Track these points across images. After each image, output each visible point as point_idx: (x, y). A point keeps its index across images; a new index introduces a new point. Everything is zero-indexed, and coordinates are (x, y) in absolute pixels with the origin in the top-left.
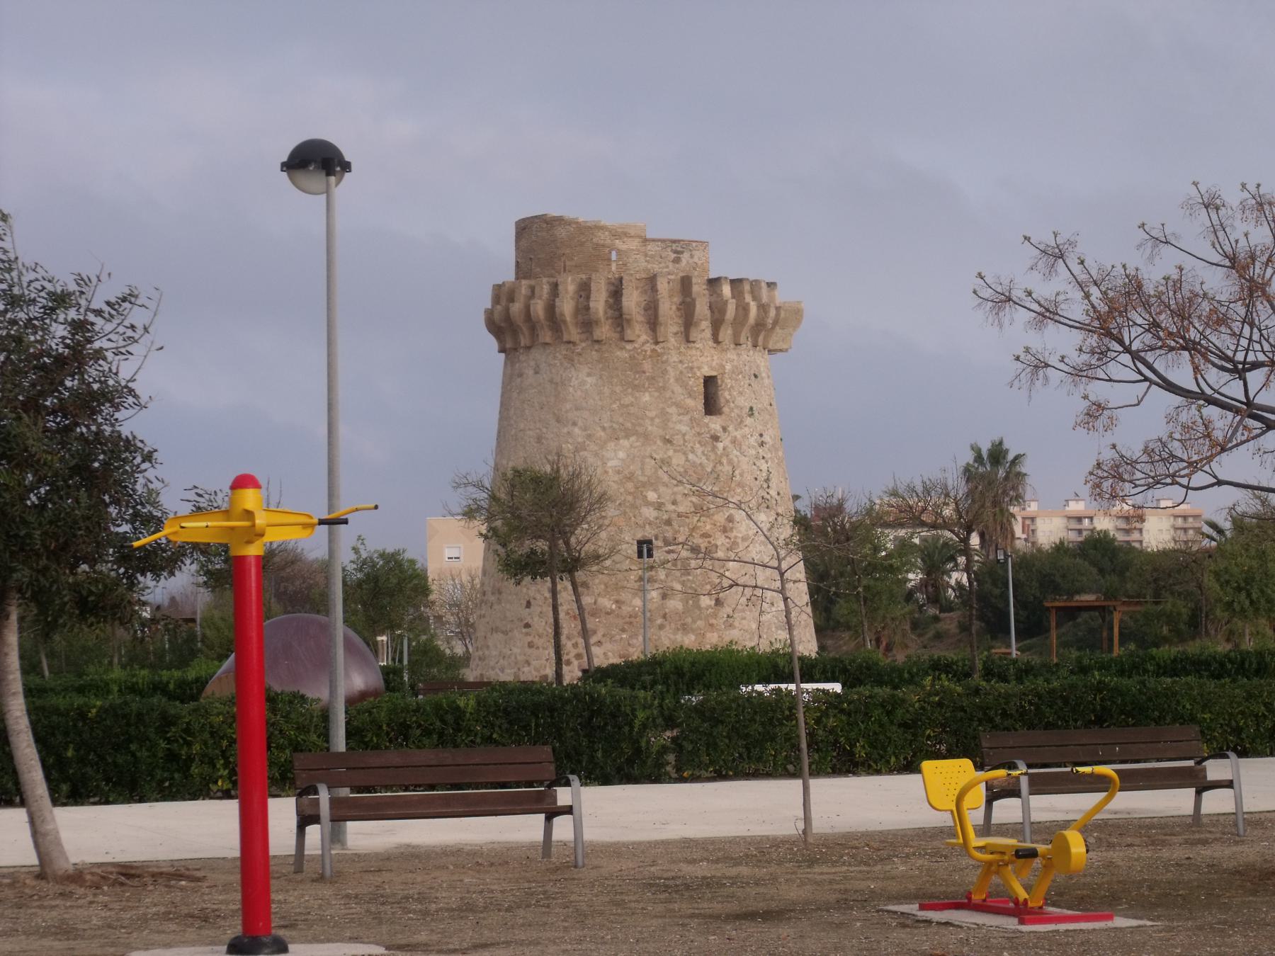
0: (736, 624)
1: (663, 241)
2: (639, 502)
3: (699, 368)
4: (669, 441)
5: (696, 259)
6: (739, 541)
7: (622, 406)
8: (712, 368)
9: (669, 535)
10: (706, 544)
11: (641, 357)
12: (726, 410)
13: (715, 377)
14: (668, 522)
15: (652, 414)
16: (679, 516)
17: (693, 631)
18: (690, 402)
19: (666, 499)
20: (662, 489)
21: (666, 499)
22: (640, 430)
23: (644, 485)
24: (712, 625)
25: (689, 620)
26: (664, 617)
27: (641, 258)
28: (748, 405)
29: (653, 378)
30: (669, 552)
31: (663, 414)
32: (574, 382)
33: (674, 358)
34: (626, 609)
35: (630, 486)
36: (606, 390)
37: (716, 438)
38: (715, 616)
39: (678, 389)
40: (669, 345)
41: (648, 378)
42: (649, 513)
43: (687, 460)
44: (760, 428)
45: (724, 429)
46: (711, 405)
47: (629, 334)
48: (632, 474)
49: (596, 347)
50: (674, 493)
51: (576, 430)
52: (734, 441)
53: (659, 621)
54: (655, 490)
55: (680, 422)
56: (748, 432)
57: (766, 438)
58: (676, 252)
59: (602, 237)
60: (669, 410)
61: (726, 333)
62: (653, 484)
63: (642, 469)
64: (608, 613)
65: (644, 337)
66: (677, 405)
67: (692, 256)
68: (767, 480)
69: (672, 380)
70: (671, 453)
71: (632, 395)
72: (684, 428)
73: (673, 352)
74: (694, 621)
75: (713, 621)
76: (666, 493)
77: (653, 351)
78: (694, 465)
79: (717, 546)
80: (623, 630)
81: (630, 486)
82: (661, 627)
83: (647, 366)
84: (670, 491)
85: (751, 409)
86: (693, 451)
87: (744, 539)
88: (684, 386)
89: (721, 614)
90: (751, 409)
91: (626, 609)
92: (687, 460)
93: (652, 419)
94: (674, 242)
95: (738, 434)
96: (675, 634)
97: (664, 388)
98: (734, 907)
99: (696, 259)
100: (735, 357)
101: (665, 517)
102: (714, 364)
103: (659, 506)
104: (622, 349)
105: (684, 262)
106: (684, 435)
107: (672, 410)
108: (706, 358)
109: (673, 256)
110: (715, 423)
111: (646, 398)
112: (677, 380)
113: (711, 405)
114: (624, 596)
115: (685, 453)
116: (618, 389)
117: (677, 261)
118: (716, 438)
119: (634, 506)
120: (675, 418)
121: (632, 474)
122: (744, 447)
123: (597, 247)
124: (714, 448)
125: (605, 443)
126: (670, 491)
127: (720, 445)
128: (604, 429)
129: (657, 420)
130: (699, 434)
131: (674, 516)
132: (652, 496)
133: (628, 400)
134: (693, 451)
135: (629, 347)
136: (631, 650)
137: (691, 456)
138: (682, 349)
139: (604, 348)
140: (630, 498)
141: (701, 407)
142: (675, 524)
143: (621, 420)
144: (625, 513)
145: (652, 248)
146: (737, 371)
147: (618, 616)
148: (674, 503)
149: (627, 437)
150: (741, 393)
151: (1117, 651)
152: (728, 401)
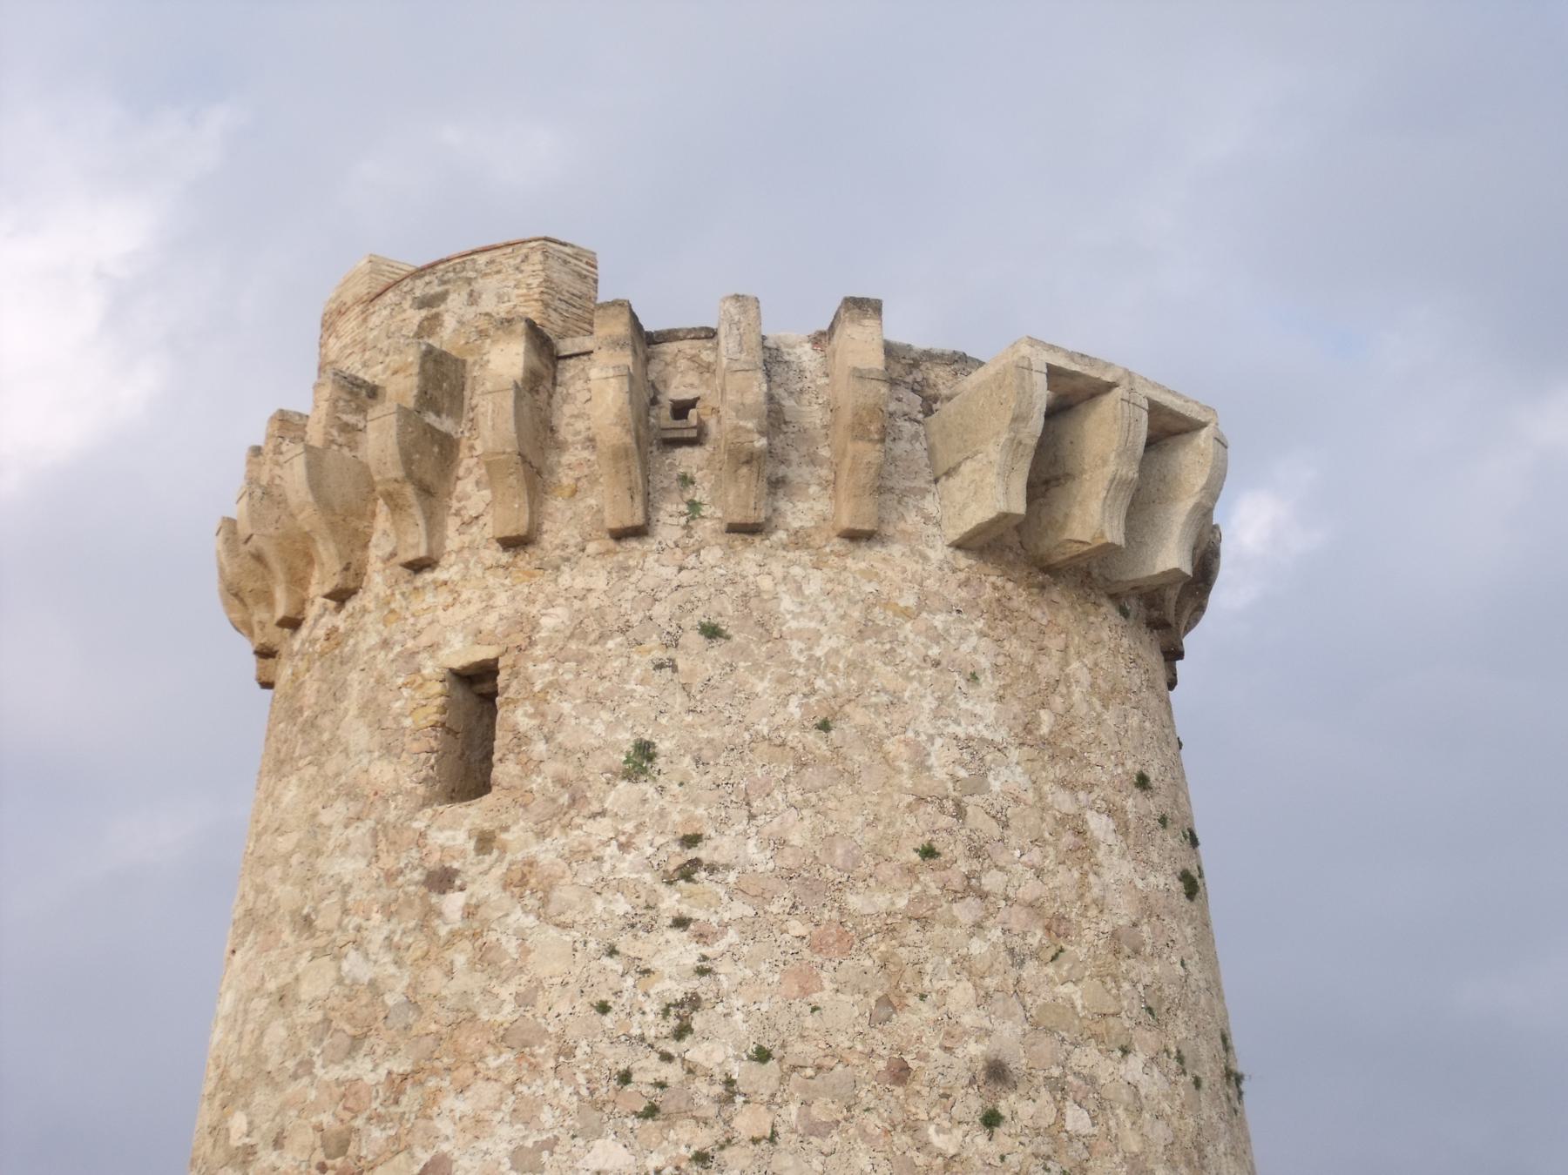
5: (488, 304)
18: (384, 773)
28: (626, 739)
45: (485, 842)
56: (624, 837)
67: (473, 299)
68: (683, 1016)
69: (353, 711)
85: (645, 751)
90: (645, 751)
95: (546, 854)
99: (488, 304)
100: (600, 582)
110: (452, 830)
118: (443, 880)
122: (564, 893)
127: (453, 903)
150: (595, 700)
152: (521, 739)
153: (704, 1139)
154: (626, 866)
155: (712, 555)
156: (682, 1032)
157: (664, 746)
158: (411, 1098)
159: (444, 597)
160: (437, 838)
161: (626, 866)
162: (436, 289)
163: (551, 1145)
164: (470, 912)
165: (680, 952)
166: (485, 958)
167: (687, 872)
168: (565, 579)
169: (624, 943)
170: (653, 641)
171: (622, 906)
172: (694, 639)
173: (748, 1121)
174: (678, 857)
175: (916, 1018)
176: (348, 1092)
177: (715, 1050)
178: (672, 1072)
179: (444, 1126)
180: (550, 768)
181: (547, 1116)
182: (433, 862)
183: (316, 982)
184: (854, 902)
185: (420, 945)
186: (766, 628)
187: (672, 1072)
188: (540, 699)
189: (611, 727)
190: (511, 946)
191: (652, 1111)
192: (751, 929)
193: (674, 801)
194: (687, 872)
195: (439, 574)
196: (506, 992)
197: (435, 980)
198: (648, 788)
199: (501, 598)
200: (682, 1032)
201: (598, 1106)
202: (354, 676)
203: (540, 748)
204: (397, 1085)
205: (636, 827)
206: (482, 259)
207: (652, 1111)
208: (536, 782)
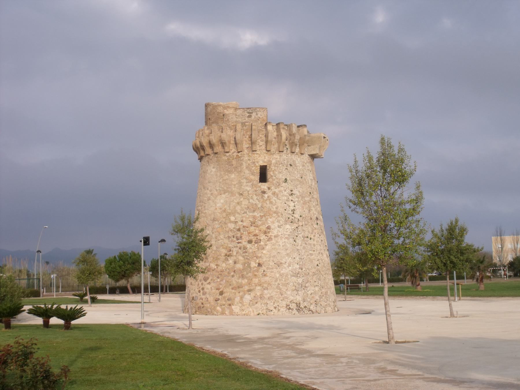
0: (268, 274)
1: (243, 109)
2: (227, 221)
3: (258, 162)
4: (241, 194)
5: (259, 115)
6: (273, 237)
7: (224, 180)
8: (264, 162)
9: (239, 235)
10: (255, 239)
11: (231, 159)
12: (270, 180)
13: (266, 166)
14: (239, 230)
15: (235, 183)
16: (244, 227)
17: (246, 278)
18: (252, 177)
19: (239, 219)
20: (237, 215)
21: (239, 219)
22: (229, 190)
23: (230, 214)
24: (256, 275)
25: (245, 273)
26: (234, 272)
27: (234, 116)
28: (284, 178)
29: (236, 167)
30: (238, 243)
31: (240, 183)
32: (209, 171)
33: (246, 158)
34: (220, 268)
35: (224, 214)
36: (218, 174)
37: (264, 192)
38: (258, 271)
39: (247, 172)
40: (244, 153)
41: (234, 168)
42: (231, 226)
43: (249, 202)
44: (291, 187)
45: (269, 188)
46: (263, 177)
47: (227, 149)
48: (225, 209)
49: (216, 155)
50: (242, 217)
51: (208, 191)
52: (274, 194)
53: (232, 274)
54: (234, 216)
55: (247, 186)
56: (284, 190)
57: (295, 192)
58: (249, 113)
59: (220, 109)
60: (242, 181)
61: (274, 148)
62: (234, 213)
63: (229, 207)
64: (213, 270)
65: (234, 150)
66: (246, 179)
67: (257, 114)
68: (293, 211)
69: (245, 168)
70: (242, 199)
71: (228, 175)
72: (248, 189)
73: (246, 156)
74: (247, 274)
75: (256, 273)
76: (239, 217)
77: (237, 156)
78: (252, 204)
79: (260, 240)
80: (218, 278)
81: (224, 214)
82: (233, 276)
83: (234, 162)
84: (240, 216)
85: (286, 179)
86: (252, 198)
87: (275, 237)
88: (250, 170)
89: (260, 270)
90: (286, 179)
91: (220, 268)
92: (249, 202)
93: (235, 185)
94: (248, 108)
95: (277, 191)
96: (238, 279)
97: (241, 171)
98: (377, 382)
99: (259, 115)
100: (278, 157)
101: (238, 228)
102: (265, 160)
103: (236, 222)
104: (225, 155)
105: (253, 117)
106: (248, 191)
107: (245, 181)
108: (262, 159)
109: (248, 114)
110: (264, 186)
111: (233, 176)
112: (247, 168)
113: (263, 177)
114: (219, 263)
115: (248, 200)
116: (222, 173)
117: (250, 116)
118: (264, 192)
119: (225, 223)
120: (245, 184)
121: (225, 209)
122: (279, 196)
123: (219, 113)
124: (263, 197)
125: (217, 196)
126: (240, 216)
127: (266, 196)
128: (217, 190)
129: (237, 185)
130: (256, 191)
131: (241, 227)
132: (232, 218)
133: (225, 178)
134: (252, 198)
135: (227, 154)
136: (221, 286)
137: (251, 201)
138: (250, 154)
139: (219, 156)
140: (224, 220)
141: (257, 178)
142: (241, 230)
143: (223, 186)
144: (222, 226)
145: (239, 112)
146: (278, 163)
147: (216, 271)
148: (242, 221)
149: (224, 193)
150: (280, 173)
151: (55, 297)
152: (272, 176)
153: (297, 225)
154: (285, 193)
155: (289, 155)
156: (293, 213)
157: (288, 179)
158: (264, 219)
159: (258, 156)
160: (263, 187)
161: (285, 193)
162: (251, 111)
163: (282, 225)
164: (268, 197)
165: (292, 204)
166: (271, 203)
167: (292, 194)
168: (274, 156)
169: (286, 202)
170: (285, 166)
171: (286, 198)
172: (289, 166)
173: (300, 224)
174: (290, 193)
175: (312, 212)
176: (254, 217)
177: (297, 216)
178: (293, 218)
179: (269, 222)
180: (276, 180)
181: (281, 222)
182: (262, 190)
183: (245, 203)
184: (306, 199)
185: (262, 200)
186: (295, 165)
187: (293, 218)
188: (273, 171)
189: (282, 176)
190: (274, 201)
191: (292, 222)
192: (298, 201)
193: (290, 186)
194: (292, 194)
195: (257, 152)
196: (274, 207)
197: (265, 205)
198: (286, 184)
199: (267, 157)
200: (293, 213)
201: (286, 221)
202: (244, 163)
203: (274, 177)
204: (261, 217)
205: (421, 246)
206: (258, 109)
207: (292, 222)
208: (274, 182)
